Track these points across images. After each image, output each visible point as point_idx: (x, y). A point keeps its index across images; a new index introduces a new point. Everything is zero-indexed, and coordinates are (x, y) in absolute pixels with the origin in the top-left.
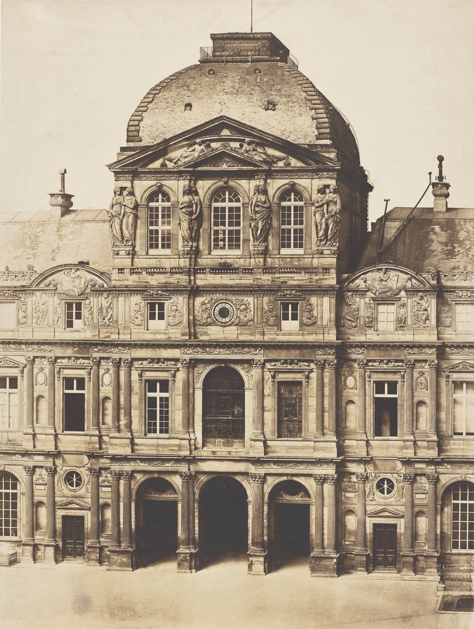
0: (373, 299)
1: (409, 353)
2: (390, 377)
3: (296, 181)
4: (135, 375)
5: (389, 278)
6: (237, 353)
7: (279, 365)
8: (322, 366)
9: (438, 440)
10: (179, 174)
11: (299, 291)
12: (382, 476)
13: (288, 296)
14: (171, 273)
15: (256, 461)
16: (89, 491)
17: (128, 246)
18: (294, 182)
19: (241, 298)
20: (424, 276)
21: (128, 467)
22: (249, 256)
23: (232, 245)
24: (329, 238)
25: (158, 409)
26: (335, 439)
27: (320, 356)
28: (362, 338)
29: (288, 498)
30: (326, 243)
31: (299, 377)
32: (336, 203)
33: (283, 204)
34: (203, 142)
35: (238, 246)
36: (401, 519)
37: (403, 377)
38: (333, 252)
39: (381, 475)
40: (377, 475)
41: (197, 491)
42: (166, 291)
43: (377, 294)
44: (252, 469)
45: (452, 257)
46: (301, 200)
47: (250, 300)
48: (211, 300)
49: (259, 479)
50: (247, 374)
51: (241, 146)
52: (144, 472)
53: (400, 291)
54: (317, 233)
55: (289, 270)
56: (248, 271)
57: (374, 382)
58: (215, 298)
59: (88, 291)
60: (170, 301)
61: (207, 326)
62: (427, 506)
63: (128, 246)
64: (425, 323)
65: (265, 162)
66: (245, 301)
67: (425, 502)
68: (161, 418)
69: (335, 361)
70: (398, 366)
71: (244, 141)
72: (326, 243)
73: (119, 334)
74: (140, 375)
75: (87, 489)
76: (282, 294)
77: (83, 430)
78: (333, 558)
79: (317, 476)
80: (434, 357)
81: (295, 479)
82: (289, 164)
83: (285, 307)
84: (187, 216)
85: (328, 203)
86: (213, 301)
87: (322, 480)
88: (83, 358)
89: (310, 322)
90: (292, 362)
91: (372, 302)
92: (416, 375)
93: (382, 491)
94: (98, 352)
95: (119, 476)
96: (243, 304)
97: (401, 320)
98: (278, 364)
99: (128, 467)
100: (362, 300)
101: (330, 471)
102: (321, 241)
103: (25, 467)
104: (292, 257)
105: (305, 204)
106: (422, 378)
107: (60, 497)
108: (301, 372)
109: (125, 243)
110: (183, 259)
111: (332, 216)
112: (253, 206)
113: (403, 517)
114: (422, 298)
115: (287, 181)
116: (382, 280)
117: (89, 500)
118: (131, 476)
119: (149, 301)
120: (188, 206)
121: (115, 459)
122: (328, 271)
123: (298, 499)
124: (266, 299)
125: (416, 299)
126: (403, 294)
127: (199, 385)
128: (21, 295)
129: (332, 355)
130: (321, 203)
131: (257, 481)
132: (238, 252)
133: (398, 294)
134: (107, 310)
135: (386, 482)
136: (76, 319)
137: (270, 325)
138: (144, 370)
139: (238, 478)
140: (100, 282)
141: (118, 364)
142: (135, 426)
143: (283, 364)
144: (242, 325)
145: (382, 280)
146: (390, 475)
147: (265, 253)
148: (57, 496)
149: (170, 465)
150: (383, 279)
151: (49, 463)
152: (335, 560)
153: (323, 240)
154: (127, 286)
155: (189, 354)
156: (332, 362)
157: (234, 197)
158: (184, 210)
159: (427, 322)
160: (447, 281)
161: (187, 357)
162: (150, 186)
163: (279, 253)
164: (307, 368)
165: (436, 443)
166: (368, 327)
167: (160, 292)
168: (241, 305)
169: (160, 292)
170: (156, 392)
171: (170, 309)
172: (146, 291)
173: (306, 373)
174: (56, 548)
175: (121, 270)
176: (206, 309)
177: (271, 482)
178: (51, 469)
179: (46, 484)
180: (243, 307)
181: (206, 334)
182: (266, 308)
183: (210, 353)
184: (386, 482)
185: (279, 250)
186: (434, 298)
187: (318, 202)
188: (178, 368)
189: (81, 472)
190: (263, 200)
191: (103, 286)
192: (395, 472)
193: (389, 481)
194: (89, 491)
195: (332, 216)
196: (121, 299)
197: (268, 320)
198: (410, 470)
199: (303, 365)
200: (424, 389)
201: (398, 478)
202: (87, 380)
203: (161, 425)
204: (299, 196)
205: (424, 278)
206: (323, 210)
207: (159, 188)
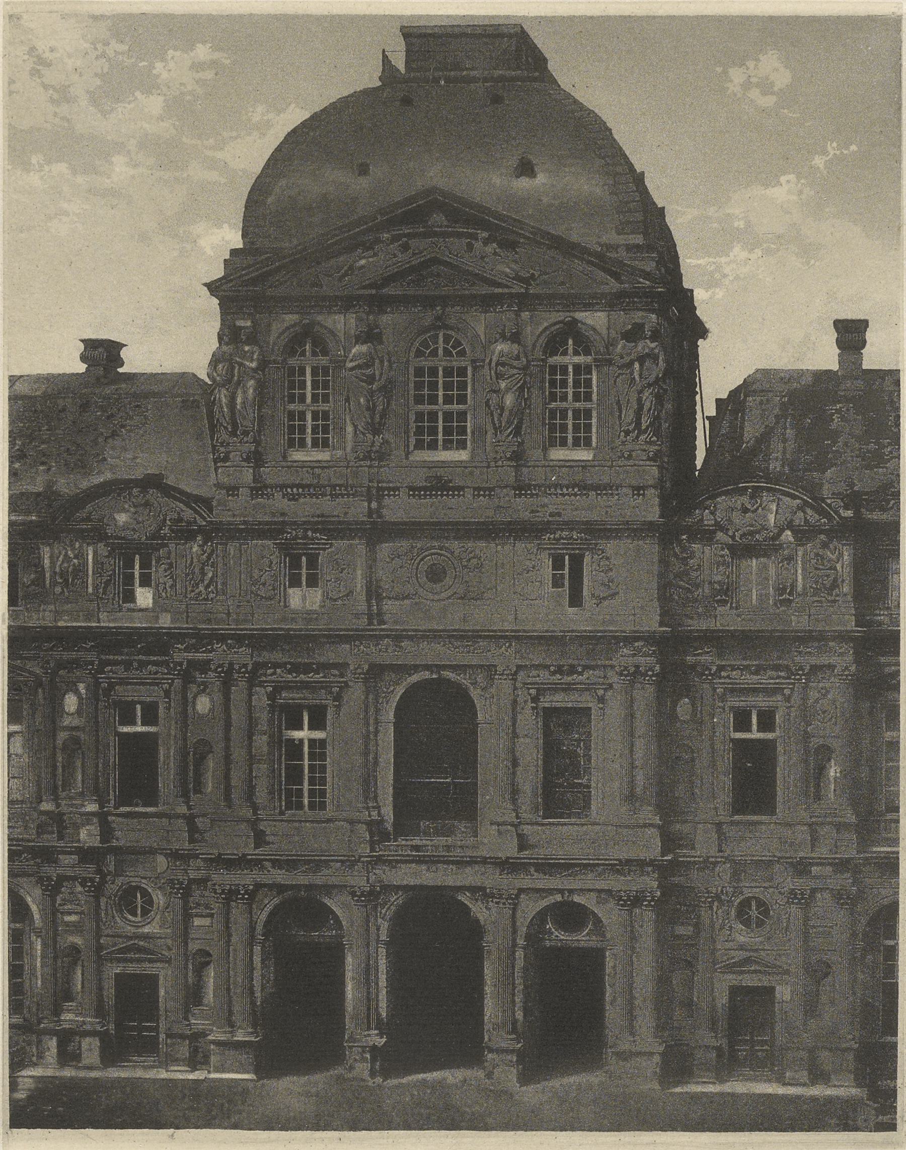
0: (731, 548)
1: (800, 653)
2: (762, 702)
3: (579, 315)
4: (261, 698)
10: (347, 303)
12: (748, 893)
14: (331, 495)
15: (507, 866)
17: (247, 442)
18: (573, 318)
21: (246, 878)
23: (451, 441)
25: (306, 762)
26: (657, 820)
27: (624, 657)
28: (704, 625)
29: (559, 936)
30: (637, 437)
31: (586, 700)
32: (655, 358)
33: (553, 360)
34: (395, 239)
35: (462, 445)
37: (788, 699)
38: (651, 454)
41: (385, 926)
42: (321, 531)
44: (491, 879)
45: (879, 464)
46: (587, 352)
49: (507, 899)
52: (281, 888)
53: (782, 531)
55: (565, 490)
57: (732, 708)
59: (166, 531)
63: (247, 442)
68: (312, 781)
69: (658, 668)
71: (474, 237)
72: (637, 437)
74: (272, 697)
76: (552, 536)
78: (651, 1054)
81: (577, 899)
83: (295, 563)
85: (641, 359)
92: (813, 695)
93: (747, 923)
96: (474, 558)
97: (784, 589)
99: (246, 878)
100: (707, 549)
101: (650, 882)
104: (567, 464)
105: (595, 360)
108: (589, 688)
111: (649, 385)
115: (561, 316)
116: (745, 510)
119: (552, 551)
120: (367, 365)
121: (220, 862)
122: (642, 492)
123: (583, 938)
127: (389, 714)
131: (504, 904)
132: (463, 455)
134: (202, 569)
135: (753, 903)
136: (140, 586)
138: (278, 689)
139: (463, 898)
140: (188, 514)
142: (261, 795)
143: (553, 673)
145: (745, 510)
147: (518, 457)
152: (657, 1059)
156: (651, 669)
157: (454, 347)
160: (872, 511)
163: (545, 459)
166: (718, 601)
168: (469, 560)
169: (310, 533)
170: (302, 729)
174: (104, 1037)
175: (232, 490)
177: (530, 908)
178: (92, 880)
180: (475, 561)
184: (753, 903)
185: (545, 450)
188: (346, 682)
191: (195, 522)
193: (761, 904)
195: (649, 385)
196: (232, 548)
203: (312, 793)
204: (583, 345)
205: (829, 505)
206: (632, 373)
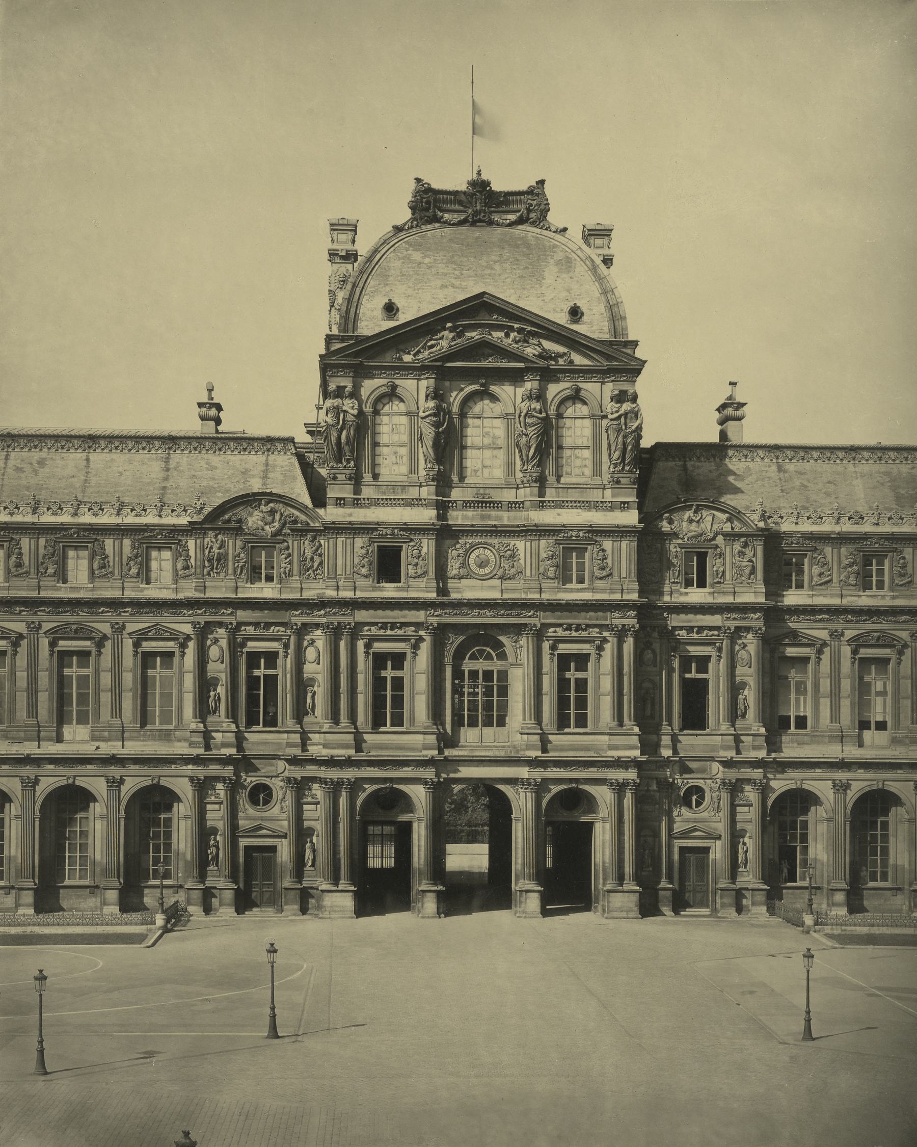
5: (701, 517)
6: (504, 615)
7: (561, 631)
8: (621, 634)
9: (767, 734)
11: (589, 532)
13: (574, 538)
16: (284, 811)
19: (506, 542)
20: (748, 515)
21: (350, 774)
22: (516, 486)
24: (626, 462)
31: (585, 648)
36: (717, 841)
37: (720, 650)
39: (690, 781)
40: (685, 781)
43: (686, 539)
47: (520, 545)
48: (465, 544)
50: (514, 644)
51: (507, 335)
52: (372, 780)
53: (716, 535)
54: (610, 454)
56: (515, 505)
58: (470, 541)
60: (411, 544)
61: (459, 579)
62: (751, 822)
64: (749, 579)
65: (540, 356)
66: (511, 546)
67: (749, 816)
70: (712, 635)
73: (338, 589)
75: (282, 808)
77: (276, 726)
79: (614, 781)
80: (761, 624)
82: (572, 362)
84: (433, 428)
86: (468, 545)
87: (620, 788)
88: (277, 624)
89: (604, 573)
90: (578, 628)
91: (679, 549)
94: (298, 616)
95: (335, 788)
98: (559, 630)
99: (350, 774)
102: (616, 465)
103: (192, 779)
106: (743, 652)
107: (244, 820)
109: (345, 464)
110: (426, 488)
112: (522, 418)
113: (719, 838)
114: (746, 545)
117: (285, 823)
118: (355, 786)
124: (543, 543)
125: (737, 547)
126: (720, 539)
128: (180, 538)
129: (633, 618)
130: (616, 415)
133: (714, 539)
137: (548, 578)
141: (335, 633)
144: (508, 579)
146: (702, 781)
148: (241, 820)
149: (410, 769)
150: (694, 518)
151: (228, 771)
153: (620, 463)
154: (350, 523)
155: (437, 616)
158: (427, 420)
159: (752, 577)
161: (434, 621)
162: (376, 387)
164: (598, 635)
165: (764, 738)
167: (396, 531)
171: (409, 554)
172: (376, 529)
173: (597, 642)
176: (458, 556)
178: (230, 779)
179: (221, 803)
181: (458, 590)
182: (543, 555)
183: (466, 615)
186: (760, 545)
187: (612, 414)
189: (273, 784)
190: (538, 407)
192: (709, 776)
194: (284, 811)
196: (340, 540)
197: (546, 570)
198: (733, 774)
199: (594, 632)
200: (746, 667)
201: (713, 785)
202: (281, 654)
207: (391, 389)
